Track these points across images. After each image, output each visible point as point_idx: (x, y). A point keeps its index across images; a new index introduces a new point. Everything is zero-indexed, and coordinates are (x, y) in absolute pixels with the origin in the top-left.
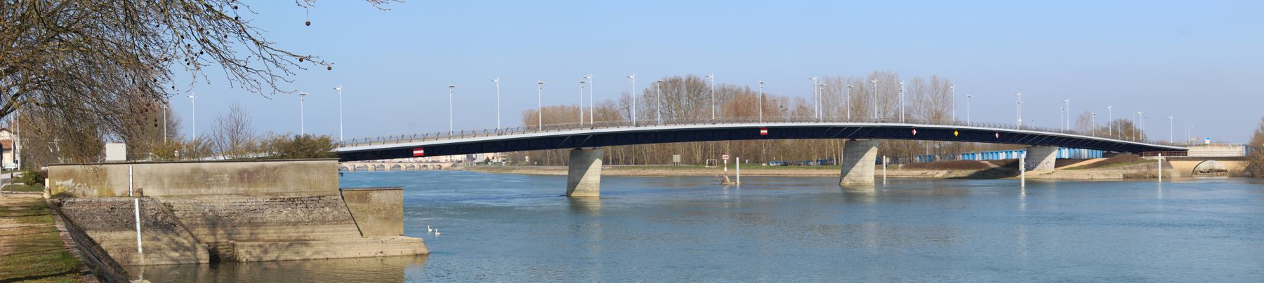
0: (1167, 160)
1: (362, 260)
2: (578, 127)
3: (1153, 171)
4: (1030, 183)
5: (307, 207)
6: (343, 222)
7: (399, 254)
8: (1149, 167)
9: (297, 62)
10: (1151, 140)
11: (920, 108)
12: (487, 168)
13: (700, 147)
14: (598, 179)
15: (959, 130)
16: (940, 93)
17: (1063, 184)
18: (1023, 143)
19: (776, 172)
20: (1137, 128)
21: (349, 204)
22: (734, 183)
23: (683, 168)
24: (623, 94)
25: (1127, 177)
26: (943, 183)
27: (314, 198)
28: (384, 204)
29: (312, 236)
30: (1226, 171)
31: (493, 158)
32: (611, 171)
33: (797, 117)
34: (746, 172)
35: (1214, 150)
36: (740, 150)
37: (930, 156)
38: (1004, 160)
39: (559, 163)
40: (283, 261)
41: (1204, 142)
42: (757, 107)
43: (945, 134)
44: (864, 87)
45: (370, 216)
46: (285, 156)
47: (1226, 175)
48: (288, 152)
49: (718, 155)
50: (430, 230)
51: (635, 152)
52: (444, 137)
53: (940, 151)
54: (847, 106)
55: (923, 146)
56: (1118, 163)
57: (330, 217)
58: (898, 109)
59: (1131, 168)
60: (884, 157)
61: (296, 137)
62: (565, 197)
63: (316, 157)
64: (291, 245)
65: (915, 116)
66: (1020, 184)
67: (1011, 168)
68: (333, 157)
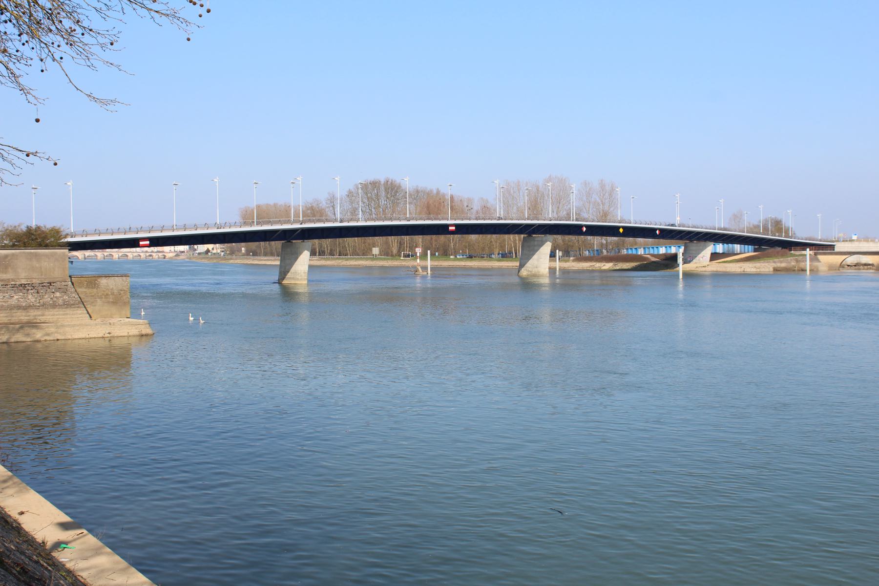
0: (815, 254)
1: (90, 340)
2: (288, 222)
3: (802, 265)
4: (687, 275)
5: (38, 293)
6: (73, 306)
7: (126, 334)
8: (797, 261)
9: (24, 157)
10: (800, 236)
11: (589, 208)
12: (207, 258)
13: (396, 241)
14: (306, 268)
15: (624, 228)
16: (607, 194)
17: (717, 276)
18: (681, 238)
19: (463, 263)
20: (787, 225)
21: (79, 290)
22: (425, 273)
23: (381, 259)
24: (329, 193)
25: (777, 270)
26: (609, 274)
27: (45, 284)
28: (112, 289)
29: (43, 319)
30: (872, 265)
31: (213, 249)
32: (318, 261)
33: (481, 215)
34: (436, 263)
35: (854, 245)
36: (431, 244)
37: (597, 250)
38: (664, 254)
39: (272, 254)
40: (15, 342)
41: (851, 238)
42: (446, 207)
43: (611, 231)
44: (540, 189)
45: (98, 300)
46: (16, 245)
47: (873, 269)
48: (19, 241)
49: (412, 248)
50: (191, 319)
51: (339, 245)
52: (168, 230)
53: (607, 245)
54: (525, 206)
55: (592, 242)
56: (768, 257)
57: (60, 302)
58: (570, 209)
59: (781, 262)
60: (557, 251)
61: (28, 227)
62: (277, 284)
63: (47, 246)
64: (22, 327)
65: (585, 215)
66: (678, 276)
67: (670, 261)
68: (63, 246)
